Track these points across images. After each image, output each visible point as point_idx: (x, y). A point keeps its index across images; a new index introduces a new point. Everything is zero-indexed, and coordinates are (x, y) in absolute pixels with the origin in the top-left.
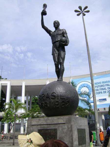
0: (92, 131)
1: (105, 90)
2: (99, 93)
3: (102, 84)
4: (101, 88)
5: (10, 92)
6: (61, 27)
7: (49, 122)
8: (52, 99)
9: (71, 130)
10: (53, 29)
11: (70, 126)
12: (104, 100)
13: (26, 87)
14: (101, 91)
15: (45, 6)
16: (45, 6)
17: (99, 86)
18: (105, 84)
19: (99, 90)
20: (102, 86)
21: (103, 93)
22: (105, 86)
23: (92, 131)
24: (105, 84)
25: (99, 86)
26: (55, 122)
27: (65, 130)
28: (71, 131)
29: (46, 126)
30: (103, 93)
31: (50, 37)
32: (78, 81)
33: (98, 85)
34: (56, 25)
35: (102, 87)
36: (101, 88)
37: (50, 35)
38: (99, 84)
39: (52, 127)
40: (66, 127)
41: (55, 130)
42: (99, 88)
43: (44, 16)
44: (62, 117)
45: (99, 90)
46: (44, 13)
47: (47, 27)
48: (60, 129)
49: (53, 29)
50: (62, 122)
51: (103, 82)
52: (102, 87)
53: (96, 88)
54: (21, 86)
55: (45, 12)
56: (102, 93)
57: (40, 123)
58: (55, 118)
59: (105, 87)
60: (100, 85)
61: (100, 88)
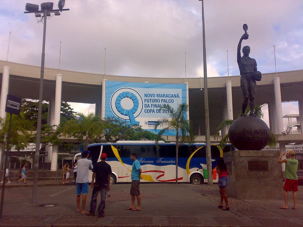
2: (150, 111)
3: (156, 98)
4: (154, 103)
5: (8, 82)
6: (251, 56)
8: (260, 135)
12: (14, 104)
13: (64, 83)
14: (153, 108)
15: (245, 27)
17: (151, 100)
18: (160, 98)
19: (150, 106)
20: (155, 101)
21: (155, 111)
25: (151, 100)
29: (257, 158)
30: (155, 111)
32: (118, 85)
33: (150, 98)
35: (156, 103)
36: (154, 103)
38: (151, 97)
39: (263, 159)
41: (266, 162)
42: (150, 104)
45: (150, 106)
51: (158, 95)
52: (156, 103)
53: (146, 103)
54: (54, 82)
56: (153, 111)
57: (250, 155)
60: (152, 98)
61: (152, 103)
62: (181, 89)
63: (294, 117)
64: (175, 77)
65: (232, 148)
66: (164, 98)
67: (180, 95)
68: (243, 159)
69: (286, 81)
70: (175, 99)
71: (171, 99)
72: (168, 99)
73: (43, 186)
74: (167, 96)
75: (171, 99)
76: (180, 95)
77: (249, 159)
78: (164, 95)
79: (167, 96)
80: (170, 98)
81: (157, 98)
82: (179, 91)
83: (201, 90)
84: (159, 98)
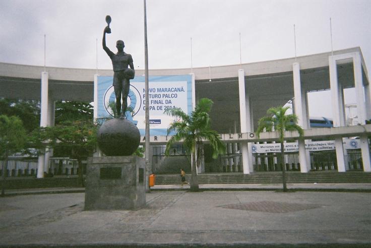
0: (52, 140)
1: (160, 105)
3: (156, 93)
4: (155, 99)
6: (126, 50)
7: (113, 161)
9: (134, 169)
10: (115, 51)
11: (134, 165)
15: (108, 19)
16: (108, 19)
18: (162, 93)
21: (156, 108)
22: (162, 96)
23: (52, 140)
24: (163, 93)
26: (120, 161)
27: (129, 169)
28: (135, 169)
30: (156, 108)
31: (110, 61)
34: (120, 45)
35: (156, 99)
36: (155, 99)
37: (111, 58)
39: (116, 166)
40: (131, 166)
41: (120, 169)
43: (106, 34)
44: (127, 157)
46: (108, 30)
47: (109, 48)
48: (125, 167)
49: (115, 51)
50: (127, 161)
51: (159, 90)
52: (156, 99)
54: (40, 80)
55: (110, 29)
58: (120, 157)
59: (161, 99)
62: (186, 82)
63: (294, 112)
64: (254, 62)
65: (207, 152)
66: (166, 93)
67: (185, 89)
68: (96, 166)
69: (306, 66)
70: (178, 93)
71: (174, 93)
72: (170, 93)
73: (222, 189)
74: (170, 90)
75: (174, 93)
76: (185, 89)
77: (102, 166)
78: (166, 90)
79: (170, 90)
80: (173, 93)
81: (158, 93)
82: (183, 84)
83: (210, 81)
84: (160, 93)
